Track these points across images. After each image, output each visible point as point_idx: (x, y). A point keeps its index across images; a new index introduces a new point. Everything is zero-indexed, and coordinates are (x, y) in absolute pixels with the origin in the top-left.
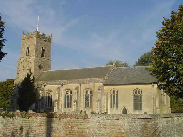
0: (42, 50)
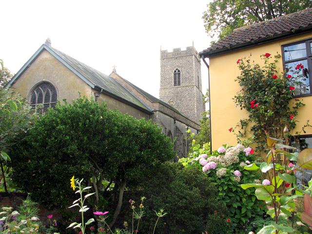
0: (175, 74)
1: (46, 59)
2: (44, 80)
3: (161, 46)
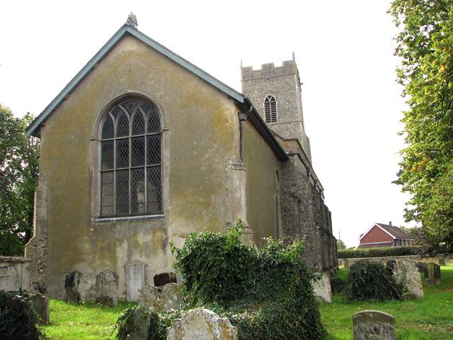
0: (267, 105)
1: (131, 53)
2: (129, 91)
3: (293, 54)
